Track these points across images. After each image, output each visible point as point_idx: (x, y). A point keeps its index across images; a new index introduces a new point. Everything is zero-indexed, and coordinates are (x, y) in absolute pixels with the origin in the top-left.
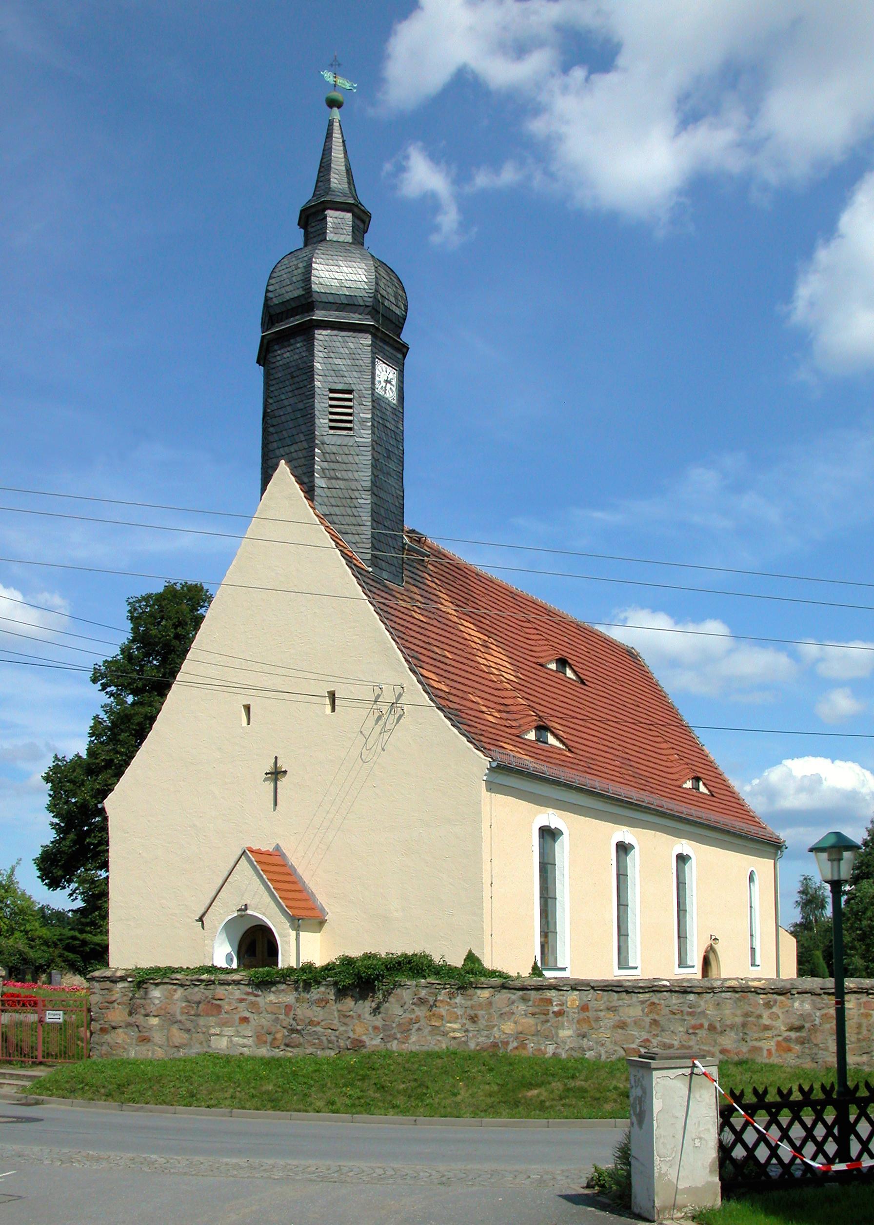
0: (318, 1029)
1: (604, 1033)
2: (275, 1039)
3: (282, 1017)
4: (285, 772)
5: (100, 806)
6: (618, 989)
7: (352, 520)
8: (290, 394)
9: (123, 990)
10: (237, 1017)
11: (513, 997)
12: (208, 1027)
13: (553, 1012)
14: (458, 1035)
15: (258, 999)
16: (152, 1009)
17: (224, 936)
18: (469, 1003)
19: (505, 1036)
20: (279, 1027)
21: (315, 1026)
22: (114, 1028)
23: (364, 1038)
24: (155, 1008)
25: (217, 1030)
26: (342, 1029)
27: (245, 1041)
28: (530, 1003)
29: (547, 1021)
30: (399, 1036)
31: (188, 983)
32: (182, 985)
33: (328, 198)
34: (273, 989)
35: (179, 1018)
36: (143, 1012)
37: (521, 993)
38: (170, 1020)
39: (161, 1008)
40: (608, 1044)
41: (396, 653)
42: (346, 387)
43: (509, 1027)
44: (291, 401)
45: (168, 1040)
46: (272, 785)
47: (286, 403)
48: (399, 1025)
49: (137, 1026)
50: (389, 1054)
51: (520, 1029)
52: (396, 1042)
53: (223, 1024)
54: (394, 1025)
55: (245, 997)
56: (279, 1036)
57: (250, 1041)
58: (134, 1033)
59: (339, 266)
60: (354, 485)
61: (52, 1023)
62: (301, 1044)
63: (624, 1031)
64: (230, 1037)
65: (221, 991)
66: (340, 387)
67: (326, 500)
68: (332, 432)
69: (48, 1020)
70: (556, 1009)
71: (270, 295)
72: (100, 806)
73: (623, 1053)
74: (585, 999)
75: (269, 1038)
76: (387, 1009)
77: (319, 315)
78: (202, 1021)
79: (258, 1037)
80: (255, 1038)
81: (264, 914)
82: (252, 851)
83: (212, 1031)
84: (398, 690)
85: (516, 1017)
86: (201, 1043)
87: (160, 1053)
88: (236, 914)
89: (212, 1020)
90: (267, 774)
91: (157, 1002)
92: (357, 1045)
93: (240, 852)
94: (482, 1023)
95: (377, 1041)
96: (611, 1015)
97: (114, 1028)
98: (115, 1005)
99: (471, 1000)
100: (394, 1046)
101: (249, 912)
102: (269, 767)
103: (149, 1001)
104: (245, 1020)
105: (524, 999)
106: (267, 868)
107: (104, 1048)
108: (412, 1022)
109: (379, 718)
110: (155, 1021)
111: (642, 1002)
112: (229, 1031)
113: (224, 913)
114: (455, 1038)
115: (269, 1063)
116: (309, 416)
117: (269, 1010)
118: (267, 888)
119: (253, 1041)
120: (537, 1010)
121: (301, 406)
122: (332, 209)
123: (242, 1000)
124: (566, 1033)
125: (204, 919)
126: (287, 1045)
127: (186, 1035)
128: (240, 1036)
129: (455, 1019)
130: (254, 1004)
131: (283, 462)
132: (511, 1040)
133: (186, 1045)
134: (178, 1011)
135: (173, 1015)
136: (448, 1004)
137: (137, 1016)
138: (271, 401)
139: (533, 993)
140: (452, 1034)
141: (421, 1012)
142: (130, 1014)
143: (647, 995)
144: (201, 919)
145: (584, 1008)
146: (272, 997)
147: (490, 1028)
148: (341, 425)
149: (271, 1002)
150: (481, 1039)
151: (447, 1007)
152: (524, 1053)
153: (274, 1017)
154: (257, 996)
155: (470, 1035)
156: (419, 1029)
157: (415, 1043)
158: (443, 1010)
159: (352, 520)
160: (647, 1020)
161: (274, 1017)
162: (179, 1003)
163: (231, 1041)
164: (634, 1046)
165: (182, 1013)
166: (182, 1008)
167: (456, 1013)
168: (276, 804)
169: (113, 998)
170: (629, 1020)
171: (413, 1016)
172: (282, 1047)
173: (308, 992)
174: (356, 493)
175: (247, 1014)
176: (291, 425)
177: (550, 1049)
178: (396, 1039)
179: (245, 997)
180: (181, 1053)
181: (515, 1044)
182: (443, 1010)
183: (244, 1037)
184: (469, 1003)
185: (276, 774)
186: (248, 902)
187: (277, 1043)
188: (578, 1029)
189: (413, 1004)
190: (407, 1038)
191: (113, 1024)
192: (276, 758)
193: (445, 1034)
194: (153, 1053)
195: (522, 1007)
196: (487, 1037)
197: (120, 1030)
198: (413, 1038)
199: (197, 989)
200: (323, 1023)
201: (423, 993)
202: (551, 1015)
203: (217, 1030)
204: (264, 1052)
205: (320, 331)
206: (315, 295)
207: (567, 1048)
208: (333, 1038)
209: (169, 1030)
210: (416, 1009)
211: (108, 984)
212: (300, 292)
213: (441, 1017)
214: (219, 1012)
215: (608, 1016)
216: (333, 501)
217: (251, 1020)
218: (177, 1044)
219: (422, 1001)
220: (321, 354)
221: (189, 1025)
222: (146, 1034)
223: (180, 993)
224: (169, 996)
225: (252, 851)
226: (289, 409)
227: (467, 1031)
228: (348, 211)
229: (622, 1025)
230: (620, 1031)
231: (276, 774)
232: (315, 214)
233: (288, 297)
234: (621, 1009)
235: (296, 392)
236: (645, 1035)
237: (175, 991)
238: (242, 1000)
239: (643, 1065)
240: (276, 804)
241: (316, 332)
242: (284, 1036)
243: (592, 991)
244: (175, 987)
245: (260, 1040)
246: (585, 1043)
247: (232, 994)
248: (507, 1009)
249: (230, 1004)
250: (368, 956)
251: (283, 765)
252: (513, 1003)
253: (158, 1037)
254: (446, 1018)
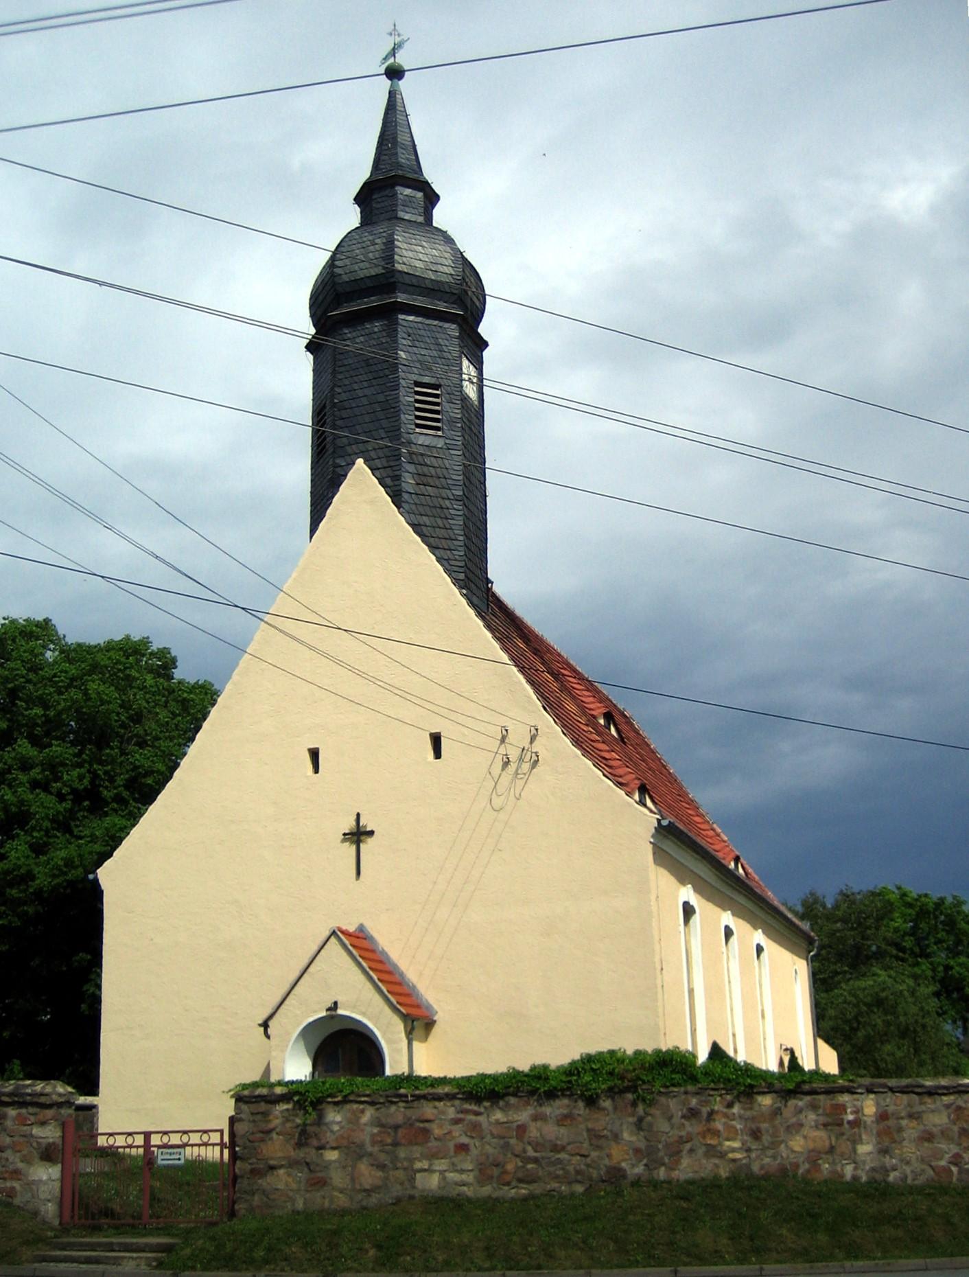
0: (562, 1156)
1: (909, 1149)
2: (505, 1172)
3: (513, 1141)
4: (371, 833)
5: (91, 877)
6: (919, 1090)
7: (442, 533)
8: (365, 384)
9: (286, 1114)
10: (451, 1145)
11: (800, 1103)
12: (411, 1161)
13: (849, 1122)
14: (738, 1156)
15: (480, 1118)
16: (330, 1138)
17: (301, 1046)
18: (748, 1113)
19: (792, 1156)
20: (509, 1155)
21: (559, 1152)
22: (272, 1168)
23: (623, 1165)
24: (333, 1137)
25: (424, 1164)
26: (594, 1154)
27: (464, 1177)
28: (821, 1111)
29: (843, 1134)
30: (666, 1160)
31: (381, 1100)
32: (372, 1103)
33: (400, 173)
34: (501, 1103)
35: (369, 1149)
36: (315, 1142)
37: (808, 1098)
38: (352, 1151)
39: (342, 1137)
40: (913, 1160)
41: (525, 690)
42: (433, 381)
43: (798, 1144)
44: (367, 392)
45: (353, 1180)
46: (354, 847)
47: (360, 393)
48: (667, 1145)
49: (307, 1164)
50: (655, 1185)
51: (811, 1145)
52: (663, 1169)
53: (433, 1156)
54: (660, 1146)
55: (461, 1116)
56: (510, 1167)
57: (468, 1178)
58: (302, 1175)
59: (423, 247)
60: (445, 493)
61: (165, 1166)
62: (540, 1178)
63: (931, 1145)
64: (442, 1172)
65: (428, 1110)
66: (426, 380)
67: (414, 507)
68: (418, 430)
69: (160, 1162)
70: (851, 1117)
71: (337, 271)
72: (91, 877)
73: (932, 1173)
74: (883, 1103)
75: (496, 1172)
76: (651, 1125)
77: (402, 298)
78: (402, 1153)
79: (480, 1170)
80: (476, 1173)
81: (364, 1014)
82: (342, 932)
83: (418, 1165)
84: (534, 731)
85: (805, 1131)
86: (402, 1184)
87: (342, 1201)
88: (324, 1014)
89: (417, 1151)
90: (345, 834)
91: (336, 1128)
92: (616, 1175)
93: (328, 933)
94: (766, 1139)
95: (639, 1169)
96: (914, 1123)
97: (272, 1168)
98: (274, 1135)
99: (751, 1109)
100: (662, 1173)
101: (340, 1012)
102: (348, 824)
103: (325, 1128)
104: (462, 1148)
105: (814, 1107)
106: (363, 953)
107: (256, 1198)
108: (682, 1141)
109: (506, 763)
110: (332, 1155)
111: (948, 1106)
112: (440, 1165)
113: (307, 1009)
114: (734, 1160)
115: (490, 1205)
116: (392, 410)
117: (495, 1132)
118: (370, 979)
119: (475, 1177)
120: (830, 1120)
121: (381, 398)
122: (402, 185)
123: (457, 1121)
124: (864, 1149)
125: (271, 1023)
126: (520, 1181)
127: (380, 1174)
128: (457, 1171)
129: (732, 1134)
130: (476, 1127)
131: (360, 461)
132: (802, 1159)
133: (379, 1187)
134: (368, 1140)
135: (361, 1146)
136: (726, 1116)
137: (307, 1150)
138: (338, 390)
139: (821, 1097)
140: (731, 1156)
141: (691, 1127)
142: (299, 1145)
143: (952, 1097)
144: (265, 1025)
145: (882, 1116)
146: (498, 1115)
147: (774, 1145)
148: (429, 422)
149: (498, 1123)
150: (767, 1160)
151: (724, 1120)
152: (818, 1177)
153: (502, 1142)
154: (477, 1114)
155: (753, 1155)
156: (691, 1151)
157: (687, 1168)
158: (719, 1125)
159: (442, 533)
160: (956, 1128)
161: (502, 1142)
162: (368, 1129)
163: (444, 1178)
164: (943, 1163)
165: (374, 1143)
166: (373, 1135)
167: (734, 1127)
168: (358, 873)
169: (271, 1126)
170: (935, 1130)
171: (683, 1133)
172: (514, 1183)
173: (541, 1105)
174: (447, 502)
175: (465, 1140)
176: (367, 418)
177: (849, 1171)
178: (664, 1164)
179: (461, 1116)
180: (374, 1199)
181: (807, 1166)
182: (719, 1125)
183: (462, 1171)
184: (748, 1113)
185: (358, 835)
186: (340, 999)
187: (507, 1178)
188: (879, 1143)
189: (683, 1117)
190: (678, 1162)
191: (272, 1162)
192: (358, 815)
193: (722, 1155)
194: (331, 1201)
195: (812, 1116)
196: (774, 1157)
197: (281, 1171)
198: (685, 1162)
199: (393, 1108)
200: (569, 1148)
201: (694, 1102)
202: (846, 1126)
203: (424, 1164)
204: (486, 1190)
205: (403, 317)
206: (397, 275)
207: (867, 1168)
208: (583, 1167)
209: (354, 1167)
210: (686, 1123)
211: (263, 1107)
212: (380, 270)
213: (717, 1133)
214: (427, 1140)
215: (912, 1125)
216: (421, 509)
217: (472, 1147)
218: (368, 1187)
219: (693, 1114)
220: (404, 342)
221: (383, 1157)
222: (319, 1175)
223: (369, 1114)
224: (354, 1120)
225: (342, 932)
226: (365, 401)
227: (749, 1150)
228: (420, 190)
229: (928, 1137)
230: (926, 1144)
231: (358, 835)
232: (381, 189)
233: (361, 274)
234: (925, 1116)
235: (374, 382)
236: (955, 1149)
237: (363, 1111)
238: (457, 1121)
239: (64, 1229)
240: (358, 873)
241: (401, 317)
242: (518, 1168)
243: (890, 1094)
244: (362, 1107)
245: (484, 1175)
246: (889, 1161)
247: (443, 1113)
248: (794, 1120)
249: (441, 1127)
250: (638, 1053)
251: (368, 823)
252: (801, 1111)
253: (338, 1178)
254: (725, 1135)
